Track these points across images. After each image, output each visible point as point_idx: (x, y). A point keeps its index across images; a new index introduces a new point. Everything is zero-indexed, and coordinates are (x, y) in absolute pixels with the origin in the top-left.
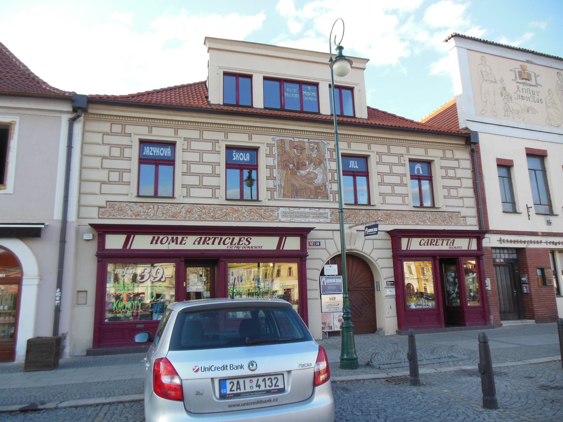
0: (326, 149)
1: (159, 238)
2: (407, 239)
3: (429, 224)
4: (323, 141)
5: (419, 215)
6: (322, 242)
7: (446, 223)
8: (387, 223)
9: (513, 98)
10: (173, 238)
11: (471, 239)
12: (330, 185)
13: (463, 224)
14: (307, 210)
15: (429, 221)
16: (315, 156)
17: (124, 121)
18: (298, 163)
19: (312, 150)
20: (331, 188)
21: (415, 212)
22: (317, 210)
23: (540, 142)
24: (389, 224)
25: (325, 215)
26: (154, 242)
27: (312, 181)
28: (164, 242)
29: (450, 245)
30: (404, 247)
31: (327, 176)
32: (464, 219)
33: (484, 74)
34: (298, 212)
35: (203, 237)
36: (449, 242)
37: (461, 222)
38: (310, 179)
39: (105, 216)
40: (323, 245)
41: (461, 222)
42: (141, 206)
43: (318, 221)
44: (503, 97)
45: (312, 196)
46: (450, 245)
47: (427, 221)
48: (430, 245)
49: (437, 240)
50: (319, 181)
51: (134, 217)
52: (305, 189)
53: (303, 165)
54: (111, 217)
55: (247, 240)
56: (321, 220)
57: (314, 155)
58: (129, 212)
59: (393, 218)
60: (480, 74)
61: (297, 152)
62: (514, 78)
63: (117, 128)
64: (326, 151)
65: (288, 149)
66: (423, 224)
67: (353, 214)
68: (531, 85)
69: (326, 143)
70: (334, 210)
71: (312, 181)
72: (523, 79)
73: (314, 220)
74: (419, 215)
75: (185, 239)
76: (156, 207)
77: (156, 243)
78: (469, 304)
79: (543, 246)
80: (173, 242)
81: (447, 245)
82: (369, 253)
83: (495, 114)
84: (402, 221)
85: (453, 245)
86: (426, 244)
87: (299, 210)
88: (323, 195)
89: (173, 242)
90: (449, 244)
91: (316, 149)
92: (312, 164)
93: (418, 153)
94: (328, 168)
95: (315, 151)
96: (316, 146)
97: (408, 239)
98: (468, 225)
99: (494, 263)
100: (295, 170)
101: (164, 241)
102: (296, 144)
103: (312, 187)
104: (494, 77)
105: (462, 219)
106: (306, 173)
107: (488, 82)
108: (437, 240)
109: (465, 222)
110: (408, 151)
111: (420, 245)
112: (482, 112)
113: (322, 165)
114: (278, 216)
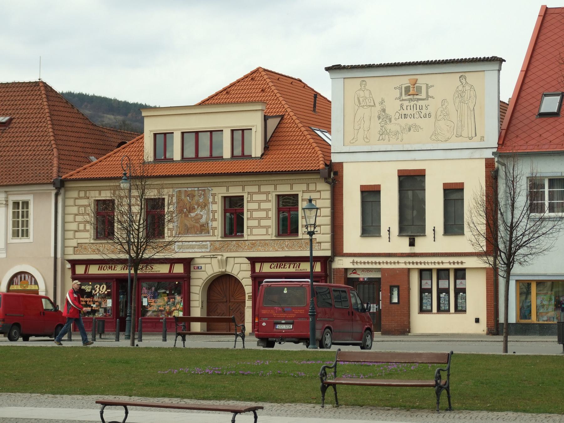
0: (210, 194)
1: (102, 266)
2: (260, 264)
3: (287, 250)
4: (208, 188)
5: (279, 243)
6: (203, 266)
7: (301, 249)
8: (252, 250)
9: (393, 120)
10: (109, 266)
11: (263, 264)
12: (211, 223)
13: (318, 249)
14: (194, 243)
15: (287, 247)
16: (202, 200)
17: (86, 190)
18: (190, 207)
19: (200, 196)
20: (212, 225)
21: (276, 241)
22: (201, 242)
23: (418, 162)
24: (254, 251)
25: (206, 247)
26: (100, 269)
27: (198, 221)
28: (105, 269)
29: (296, 268)
30: (257, 270)
31: (209, 216)
32: (320, 244)
33: (361, 99)
34: (188, 245)
35: (279, 264)
36: (296, 265)
37: (316, 247)
38: (197, 219)
39: (78, 253)
40: (203, 269)
41: (316, 247)
42: (96, 245)
43: (201, 251)
44: (381, 120)
45: (198, 233)
46: (296, 268)
47: (285, 248)
48: (279, 268)
49: (285, 264)
50: (203, 220)
51: (92, 253)
52: (194, 227)
53: (193, 209)
54: (80, 253)
55: (151, 267)
56: (203, 250)
57: (201, 201)
58: (90, 250)
59: (257, 246)
60: (357, 101)
61: (190, 199)
62: (398, 95)
63: (82, 194)
64: (210, 195)
65: (183, 197)
66: (281, 250)
67: (226, 245)
68: (419, 100)
69: (210, 189)
70: (213, 242)
71: (198, 221)
72: (409, 95)
73: (198, 250)
74: (279, 243)
75: (116, 267)
76: (104, 245)
77: (101, 270)
78: (121, 296)
79: (402, 266)
80: (110, 269)
81: (294, 268)
82: (230, 272)
83: (368, 140)
84: (264, 248)
85: (299, 268)
86: (275, 267)
87: (189, 244)
88: (205, 231)
89: (110, 269)
90: (295, 267)
91: (203, 195)
92: (199, 208)
93: (284, 190)
94: (211, 209)
95: (202, 197)
96: (203, 193)
97: (260, 263)
98: (322, 250)
99: (74, 276)
100: (188, 213)
101: (105, 268)
102: (189, 193)
103: (198, 225)
104: (373, 100)
105: (317, 244)
106: (195, 215)
107: (365, 107)
108: (285, 264)
109: (319, 247)
110: (275, 189)
111: (271, 268)
112: (352, 142)
113: (206, 208)
114: (174, 249)
